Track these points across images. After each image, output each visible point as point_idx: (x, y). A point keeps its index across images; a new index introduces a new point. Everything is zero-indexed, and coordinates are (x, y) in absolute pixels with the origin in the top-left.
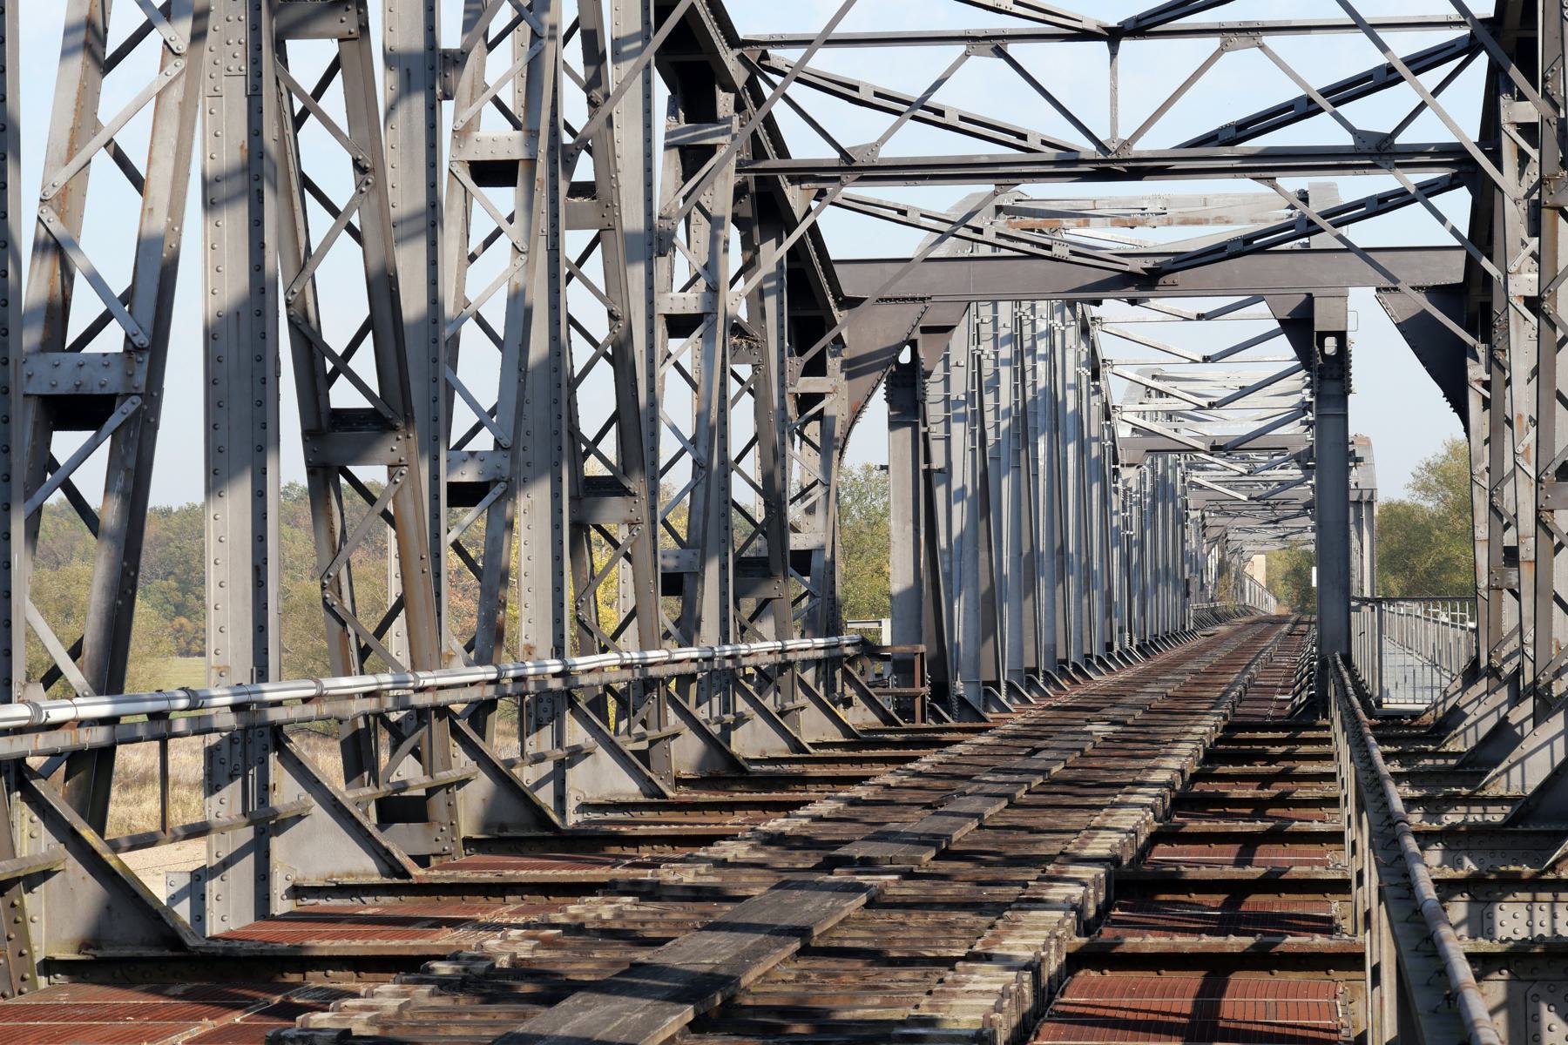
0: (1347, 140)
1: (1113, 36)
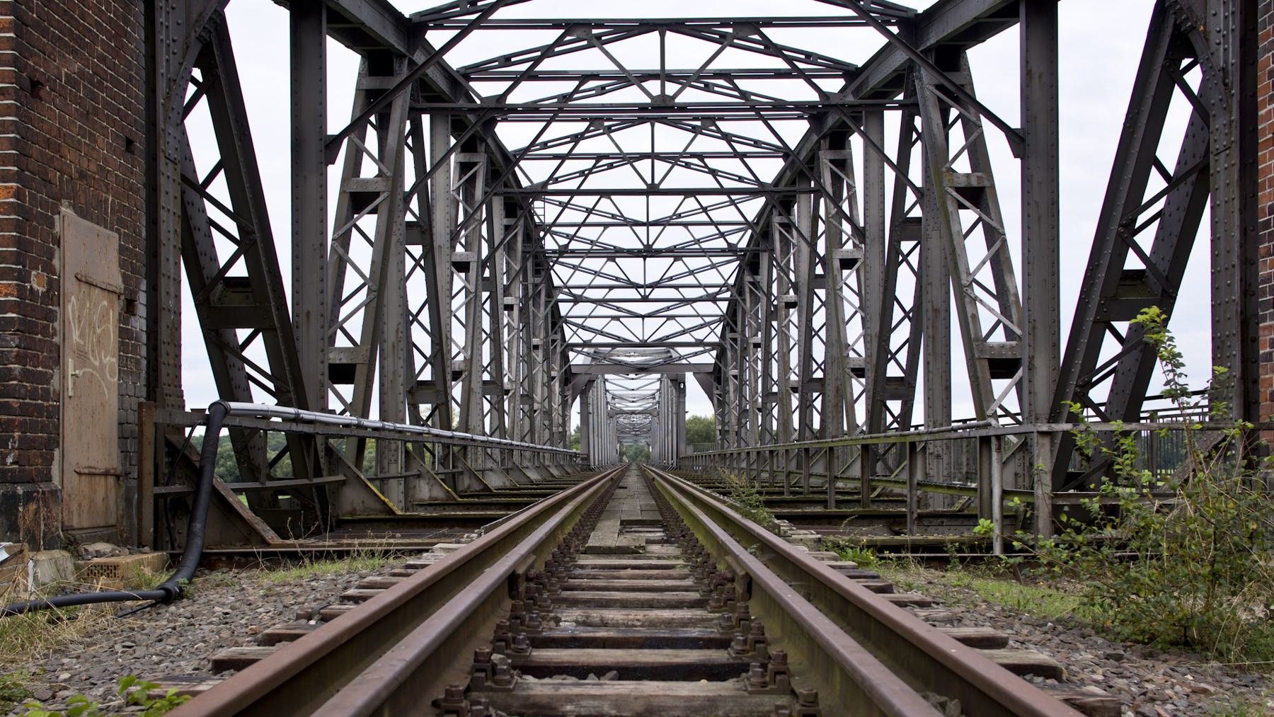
0: (693, 341)
1: (643, 317)
